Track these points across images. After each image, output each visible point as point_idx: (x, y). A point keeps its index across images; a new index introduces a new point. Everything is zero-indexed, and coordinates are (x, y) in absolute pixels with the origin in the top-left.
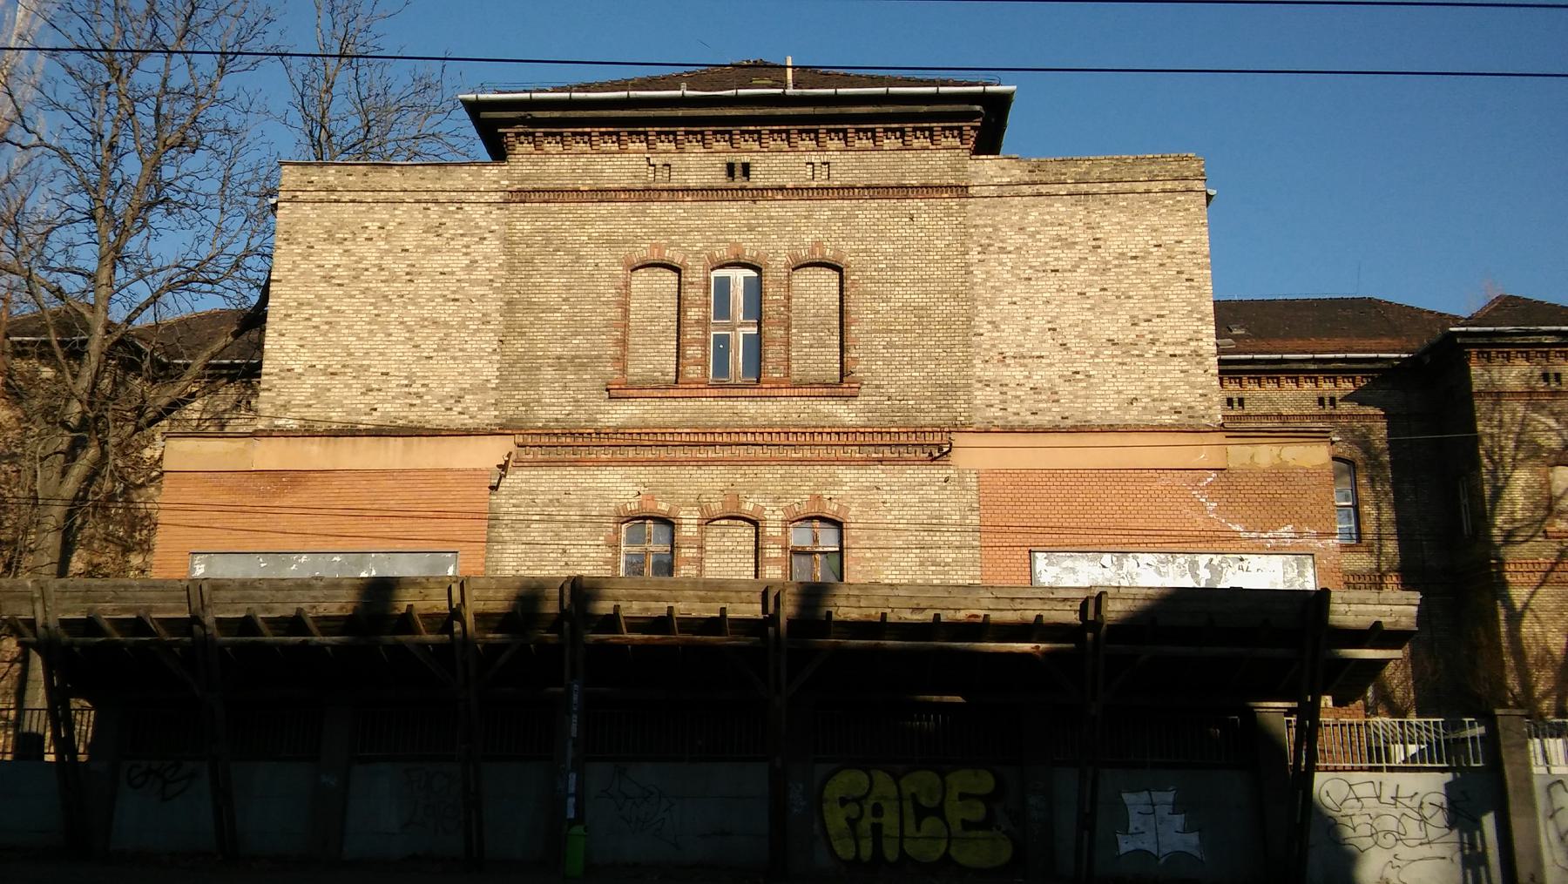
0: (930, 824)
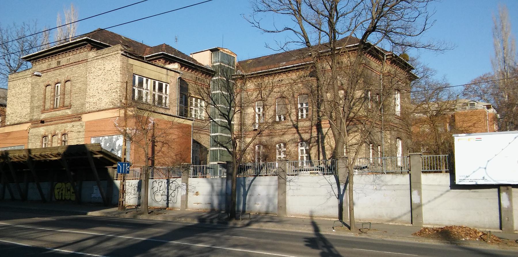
0: (69, 192)
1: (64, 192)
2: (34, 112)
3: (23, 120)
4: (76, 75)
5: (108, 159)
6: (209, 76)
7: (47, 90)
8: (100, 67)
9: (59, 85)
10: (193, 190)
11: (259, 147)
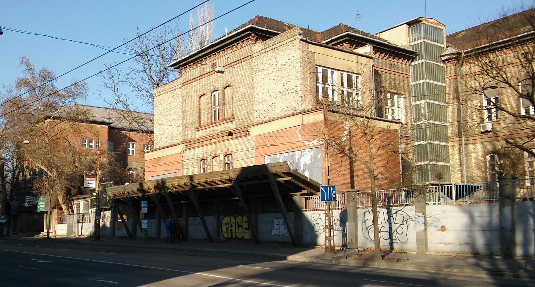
0: (240, 228)
1: (234, 228)
2: (187, 130)
3: (175, 142)
4: (239, 78)
5: (297, 183)
6: (408, 60)
7: (201, 101)
8: (270, 62)
9: (216, 93)
10: (436, 223)
11: (492, 157)
